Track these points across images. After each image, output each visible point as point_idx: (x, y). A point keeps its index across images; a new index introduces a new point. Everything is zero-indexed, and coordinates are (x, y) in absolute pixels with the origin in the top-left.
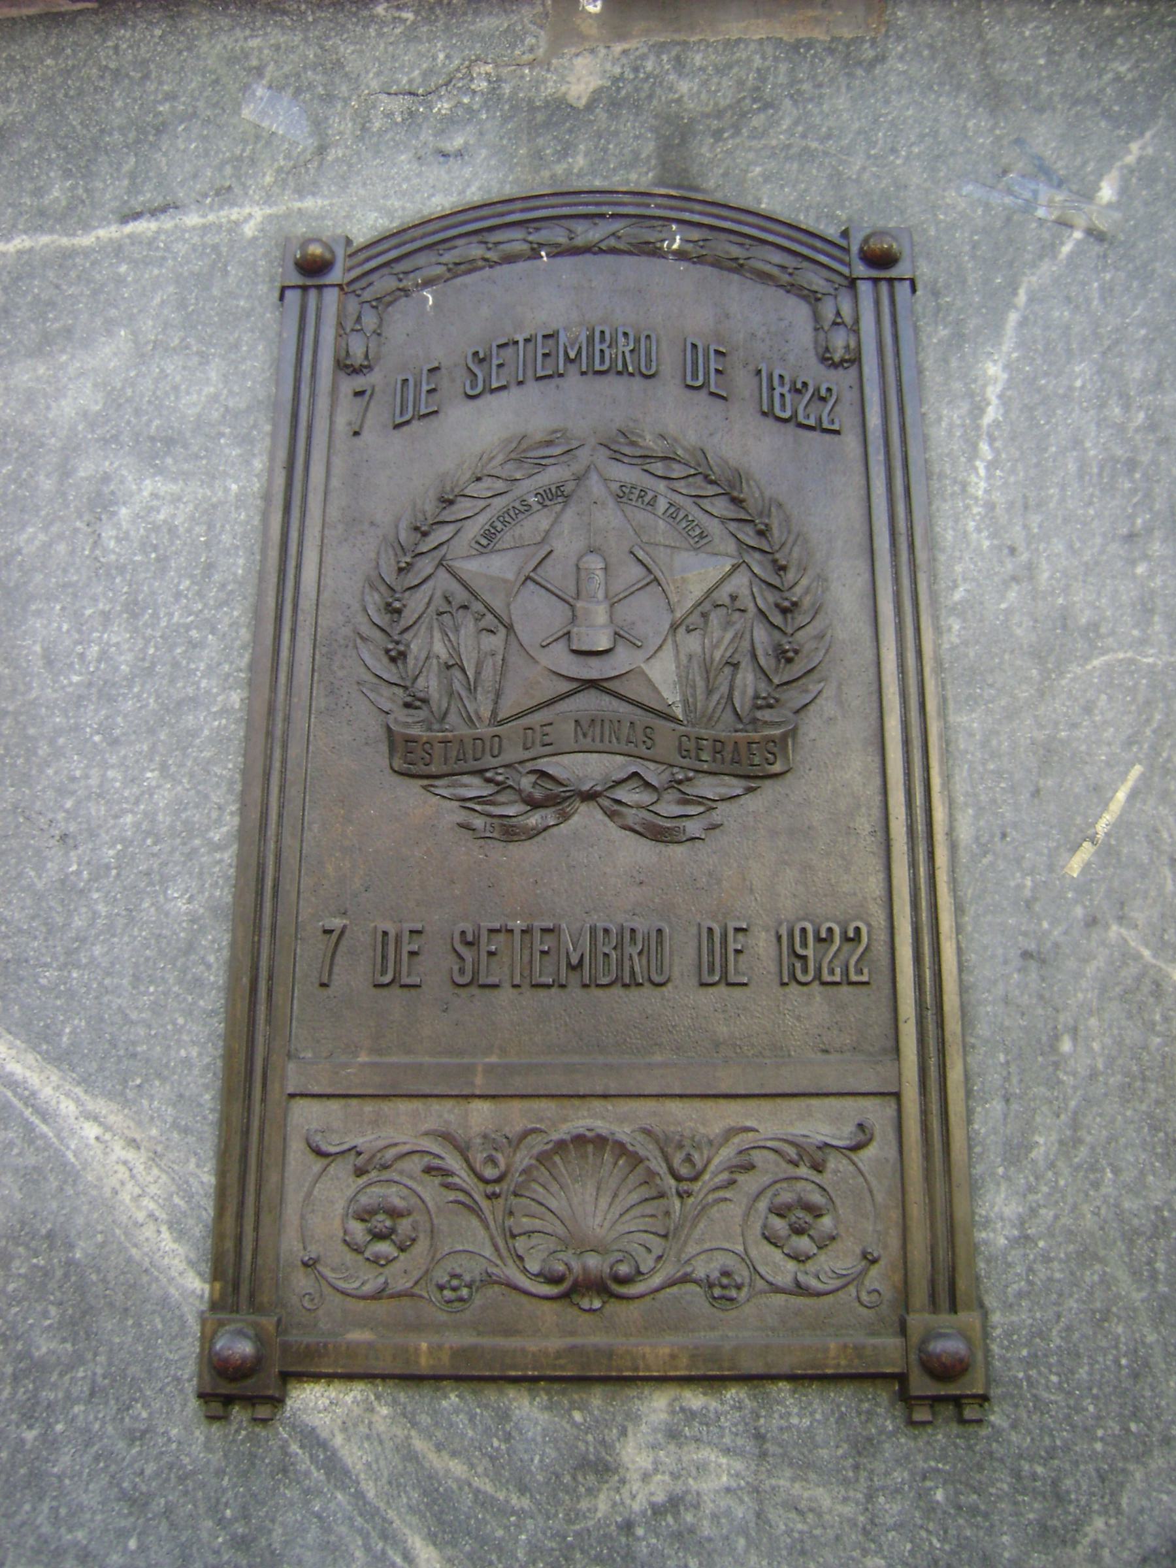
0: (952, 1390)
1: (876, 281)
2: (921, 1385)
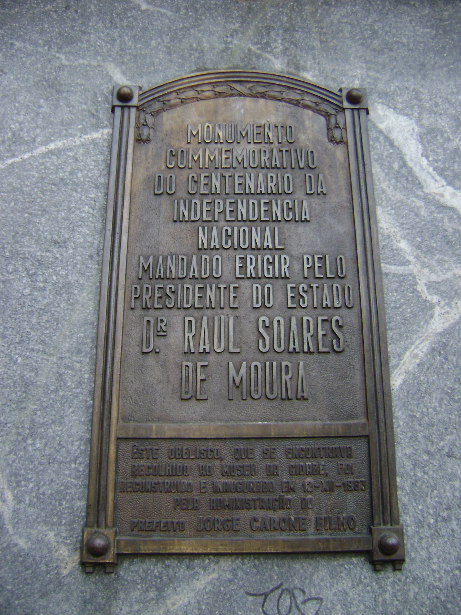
0: (100, 560)
1: (123, 107)
2: (379, 556)
